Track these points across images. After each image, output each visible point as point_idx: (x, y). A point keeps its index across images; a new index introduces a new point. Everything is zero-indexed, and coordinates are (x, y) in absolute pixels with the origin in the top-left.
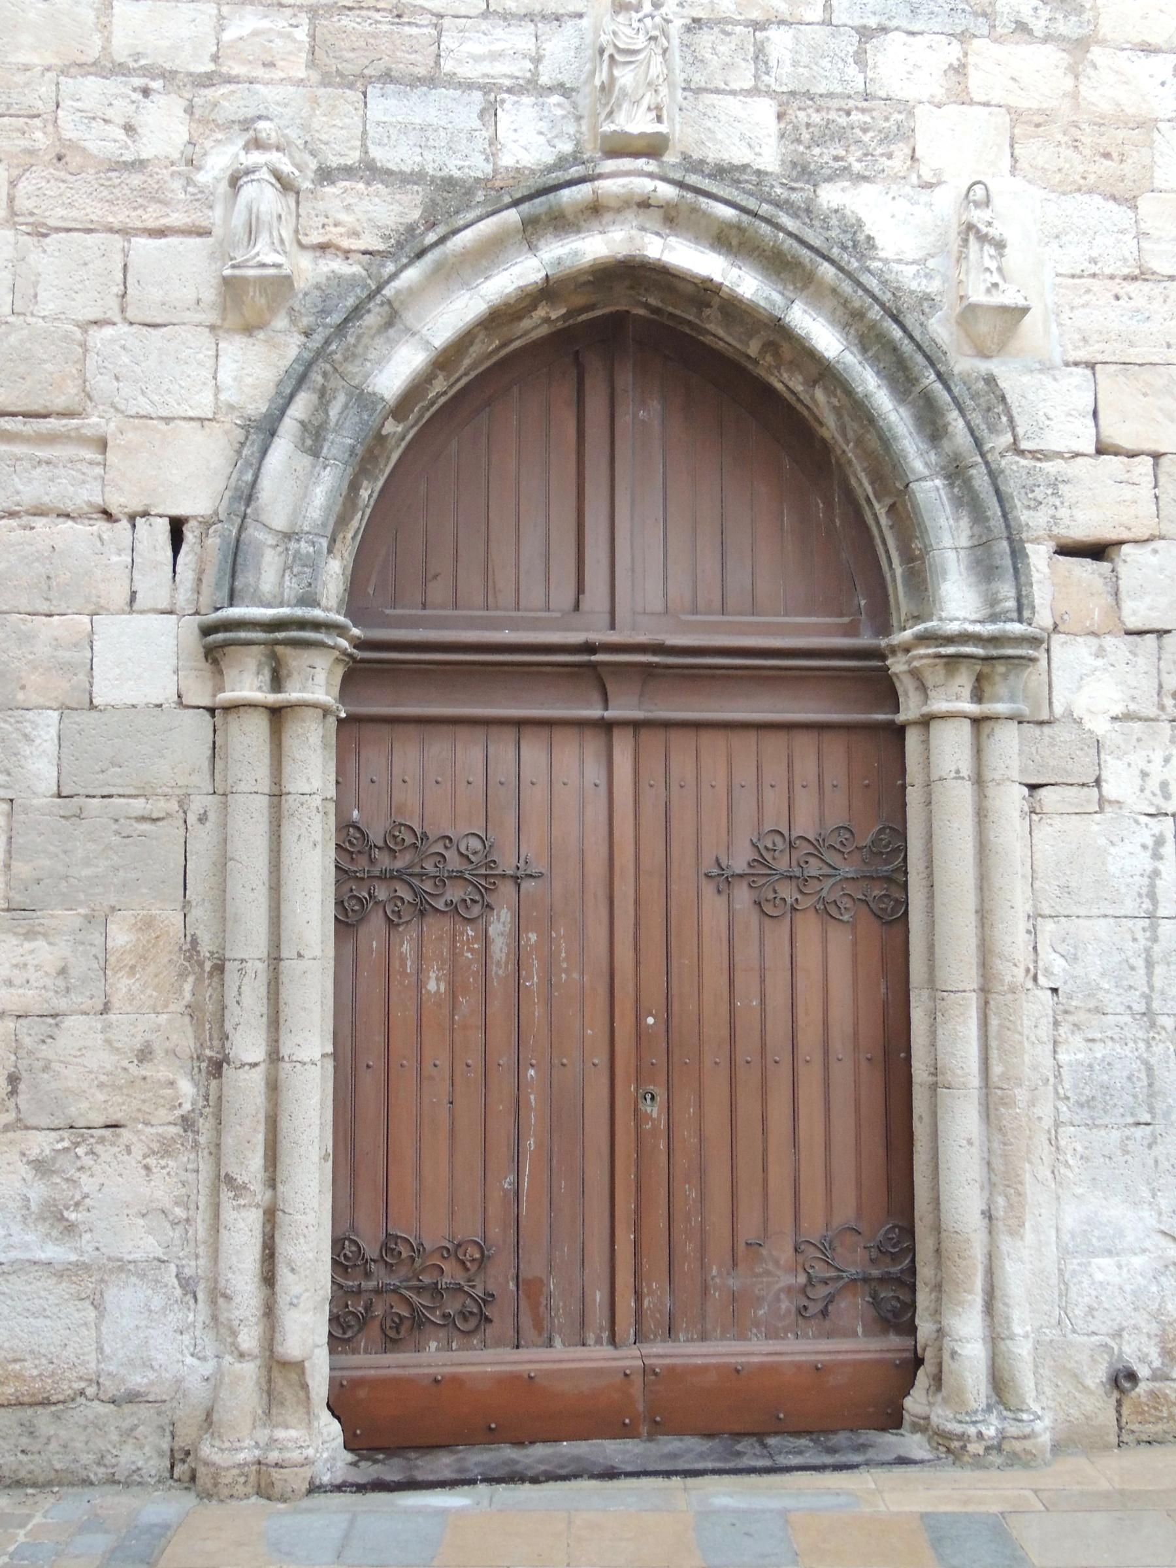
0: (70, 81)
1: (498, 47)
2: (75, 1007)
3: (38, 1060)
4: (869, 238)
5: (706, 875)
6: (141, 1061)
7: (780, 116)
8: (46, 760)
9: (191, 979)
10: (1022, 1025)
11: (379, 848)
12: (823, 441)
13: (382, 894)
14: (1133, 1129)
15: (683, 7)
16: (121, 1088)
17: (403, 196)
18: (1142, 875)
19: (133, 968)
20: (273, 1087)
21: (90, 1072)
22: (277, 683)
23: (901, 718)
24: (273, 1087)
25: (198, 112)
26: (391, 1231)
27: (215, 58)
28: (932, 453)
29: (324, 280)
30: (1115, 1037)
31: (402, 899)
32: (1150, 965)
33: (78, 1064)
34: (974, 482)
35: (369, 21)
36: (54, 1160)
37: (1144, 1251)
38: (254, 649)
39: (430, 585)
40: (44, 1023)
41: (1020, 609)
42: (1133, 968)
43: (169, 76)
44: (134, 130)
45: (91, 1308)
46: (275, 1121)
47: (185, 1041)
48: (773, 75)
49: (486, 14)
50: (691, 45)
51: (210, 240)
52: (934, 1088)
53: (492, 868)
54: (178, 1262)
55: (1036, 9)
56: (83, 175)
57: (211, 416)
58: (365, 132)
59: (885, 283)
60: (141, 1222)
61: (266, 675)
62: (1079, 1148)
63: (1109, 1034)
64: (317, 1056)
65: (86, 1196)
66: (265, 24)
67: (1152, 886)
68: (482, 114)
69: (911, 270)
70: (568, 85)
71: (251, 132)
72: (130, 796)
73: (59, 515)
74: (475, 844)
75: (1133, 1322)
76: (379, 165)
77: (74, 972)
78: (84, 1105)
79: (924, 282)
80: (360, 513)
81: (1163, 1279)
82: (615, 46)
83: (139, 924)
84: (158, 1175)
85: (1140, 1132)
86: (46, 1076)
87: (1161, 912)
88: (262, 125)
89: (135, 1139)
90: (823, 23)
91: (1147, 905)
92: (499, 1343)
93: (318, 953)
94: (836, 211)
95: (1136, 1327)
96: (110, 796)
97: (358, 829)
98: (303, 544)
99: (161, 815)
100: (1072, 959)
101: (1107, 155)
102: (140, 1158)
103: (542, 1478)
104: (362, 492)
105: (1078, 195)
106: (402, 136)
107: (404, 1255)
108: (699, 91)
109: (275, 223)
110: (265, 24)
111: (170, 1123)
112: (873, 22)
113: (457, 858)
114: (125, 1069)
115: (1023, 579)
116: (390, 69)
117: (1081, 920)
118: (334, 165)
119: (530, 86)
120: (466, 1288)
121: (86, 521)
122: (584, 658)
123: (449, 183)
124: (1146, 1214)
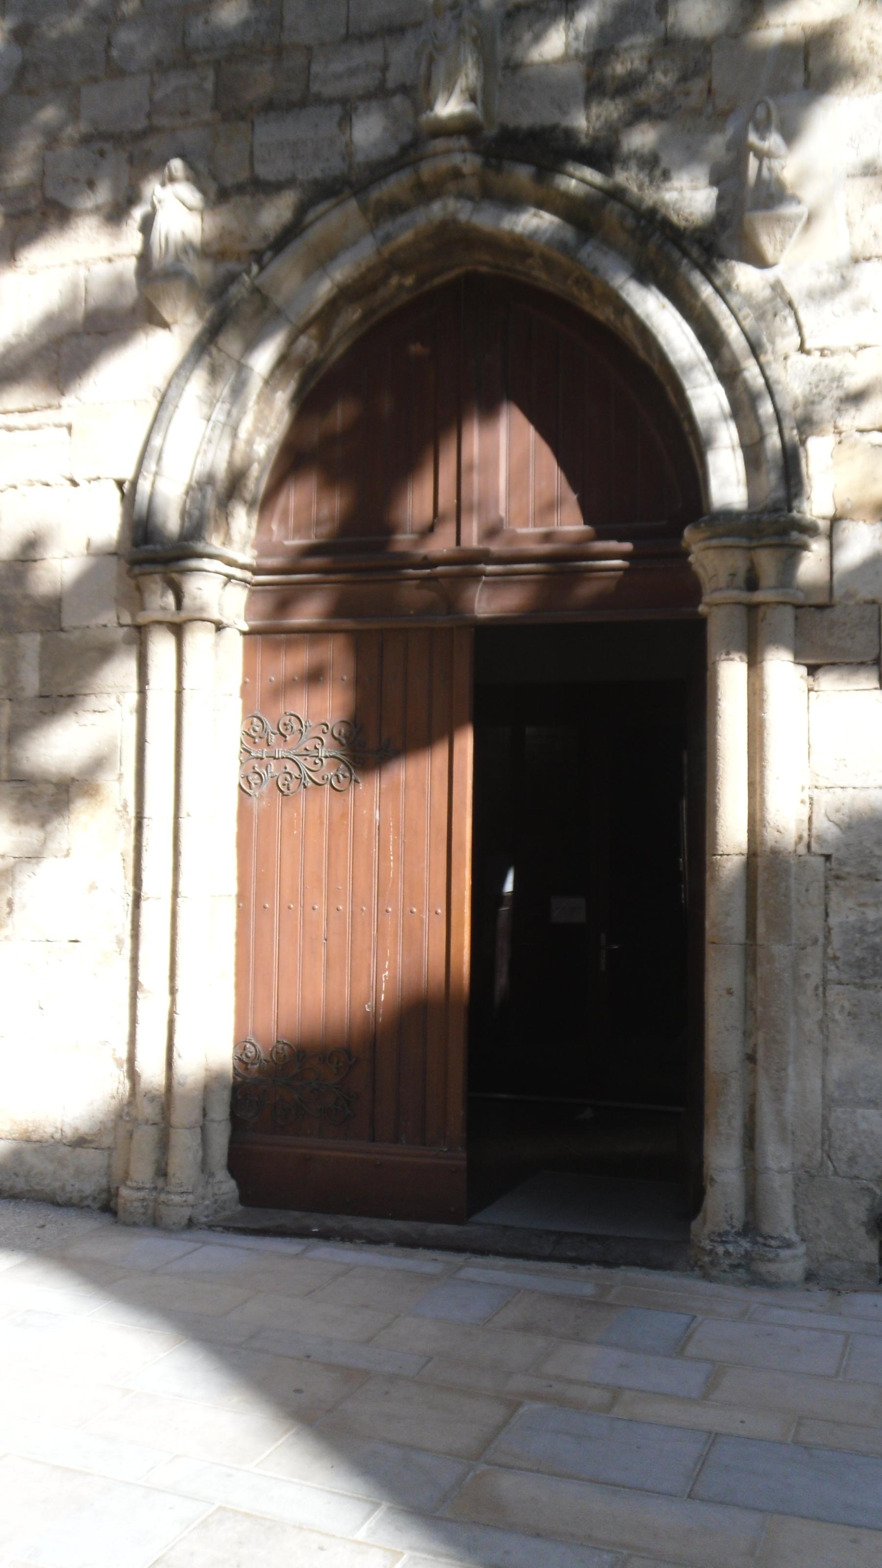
62: (847, 1005)
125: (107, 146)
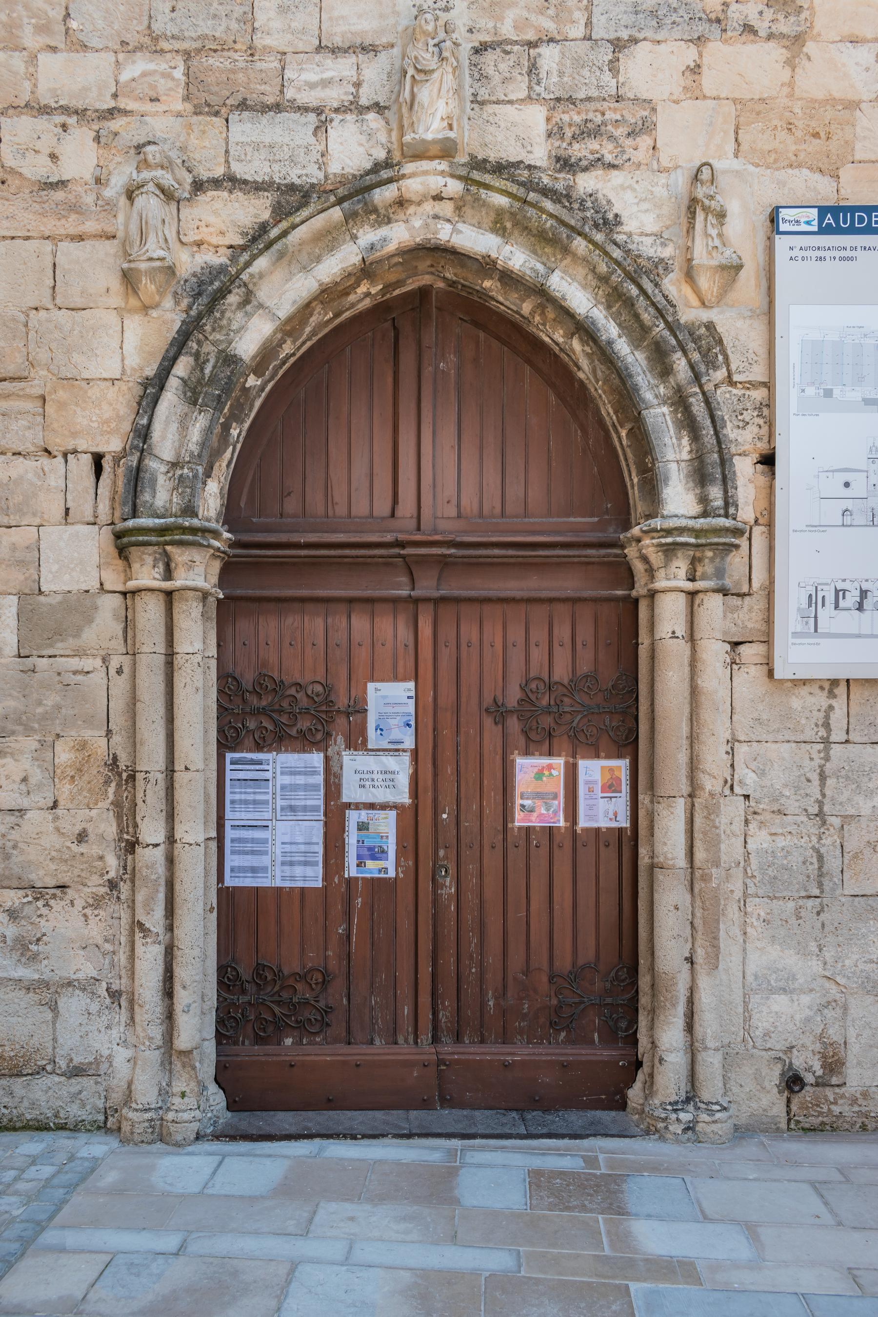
0: (9, 120)
1: (328, 75)
2: (33, 805)
3: (9, 841)
4: (616, 216)
5: (487, 710)
6: (80, 842)
7: (548, 120)
8: (9, 631)
9: (113, 785)
10: (720, 823)
11: (250, 692)
12: (581, 382)
13: (252, 724)
14: (805, 900)
15: (472, 32)
16: (66, 861)
17: (257, 201)
18: (819, 710)
19: (73, 777)
20: (170, 860)
21: (45, 849)
22: (168, 575)
23: (634, 593)
24: (170, 860)
25: (103, 140)
26: (259, 962)
27: (115, 96)
28: (662, 386)
29: (199, 271)
30: (793, 832)
31: (266, 728)
32: (823, 777)
33: (36, 844)
34: (693, 408)
35: (230, 60)
36: (22, 909)
37: (811, 990)
38: (151, 549)
39: (285, 500)
40: (13, 815)
41: (727, 505)
42: (809, 781)
43: (80, 113)
44: (57, 157)
45: (49, 1011)
46: (172, 885)
47: (111, 829)
48: (543, 85)
49: (320, 48)
50: (478, 64)
51: (115, 242)
52: (652, 867)
53: (330, 706)
54: (108, 981)
55: (761, 13)
56: (21, 194)
57: (118, 377)
58: (227, 152)
59: (628, 252)
60: (82, 952)
61: (161, 567)
62: (762, 914)
63: (789, 829)
64: (201, 839)
65: (44, 935)
66: (152, 66)
67: (827, 717)
68: (315, 133)
69: (648, 241)
70: (382, 104)
71: (142, 155)
72: (68, 656)
73: (14, 454)
74: (319, 688)
75: (801, 1042)
76: (238, 177)
77: (33, 781)
78: (41, 873)
79: (659, 249)
80: (231, 448)
81: (826, 1011)
82: (416, 68)
83: (77, 747)
84: (92, 921)
85: (810, 903)
86: (15, 852)
87: (832, 739)
88: (150, 149)
89: (76, 897)
90: (584, 39)
91: (822, 732)
92: (336, 1040)
93: (201, 766)
94: (591, 195)
95: (803, 1046)
96: (55, 656)
97: (235, 678)
98: (186, 471)
99: (90, 669)
100: (761, 773)
101: (816, 135)
102: (81, 909)
103: (359, 1136)
104: (232, 431)
105: (790, 171)
106: (256, 152)
107: (269, 978)
108: (482, 103)
109: (160, 226)
110: (152, 66)
111: (100, 885)
112: (624, 35)
113: (305, 699)
114: (68, 848)
115: (730, 484)
116: (245, 99)
117: (768, 744)
118: (205, 179)
119: (355, 107)
120: (312, 1002)
121: (33, 458)
122: (396, 551)
123: (292, 188)
124: (814, 963)
125: (72, 120)
